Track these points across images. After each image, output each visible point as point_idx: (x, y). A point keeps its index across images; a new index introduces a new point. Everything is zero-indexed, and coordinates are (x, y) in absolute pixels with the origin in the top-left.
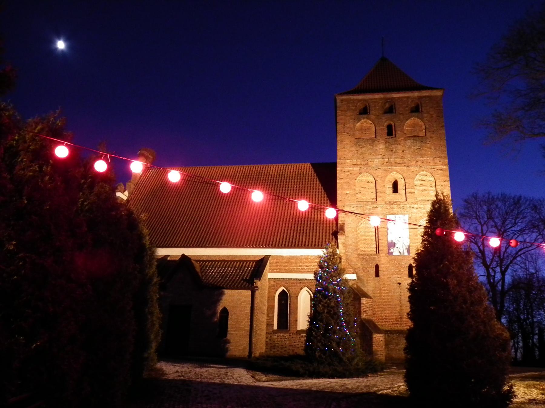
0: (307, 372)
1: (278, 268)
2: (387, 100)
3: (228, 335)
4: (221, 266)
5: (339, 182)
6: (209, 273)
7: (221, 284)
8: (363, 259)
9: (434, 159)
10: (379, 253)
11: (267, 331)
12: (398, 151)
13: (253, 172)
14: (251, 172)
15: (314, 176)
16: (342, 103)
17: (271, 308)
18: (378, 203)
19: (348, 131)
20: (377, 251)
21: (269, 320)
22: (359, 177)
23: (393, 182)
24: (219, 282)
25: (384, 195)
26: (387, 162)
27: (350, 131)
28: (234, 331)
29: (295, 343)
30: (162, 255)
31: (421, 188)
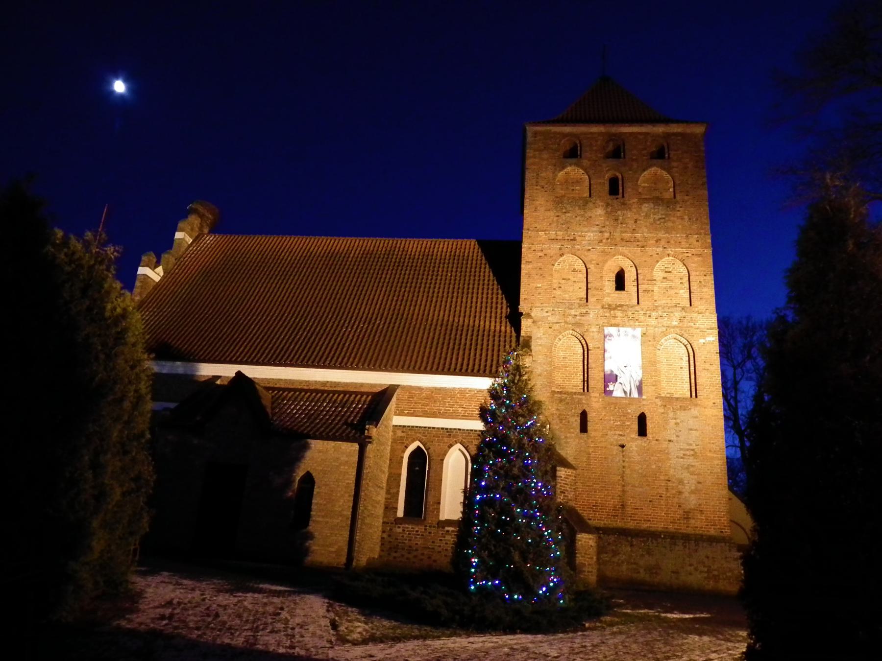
0: (457, 617)
1: (412, 408)
2: (611, 137)
3: (310, 524)
4: (311, 399)
5: (525, 268)
6: (287, 410)
7: (305, 430)
8: (561, 401)
9: (687, 236)
10: (588, 391)
11: (385, 520)
12: (627, 221)
13: (380, 249)
14: (376, 249)
15: (481, 260)
16: (535, 137)
17: (394, 479)
18: (590, 307)
19: (543, 184)
20: (586, 388)
21: (390, 499)
22: (559, 261)
23: (616, 272)
24: (302, 426)
25: (600, 293)
26: (608, 239)
27: (546, 184)
28: (323, 517)
29: (433, 542)
30: (208, 376)
31: (664, 285)
